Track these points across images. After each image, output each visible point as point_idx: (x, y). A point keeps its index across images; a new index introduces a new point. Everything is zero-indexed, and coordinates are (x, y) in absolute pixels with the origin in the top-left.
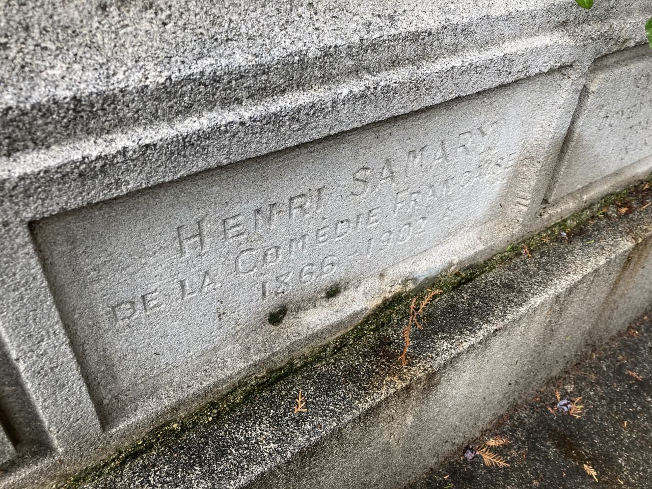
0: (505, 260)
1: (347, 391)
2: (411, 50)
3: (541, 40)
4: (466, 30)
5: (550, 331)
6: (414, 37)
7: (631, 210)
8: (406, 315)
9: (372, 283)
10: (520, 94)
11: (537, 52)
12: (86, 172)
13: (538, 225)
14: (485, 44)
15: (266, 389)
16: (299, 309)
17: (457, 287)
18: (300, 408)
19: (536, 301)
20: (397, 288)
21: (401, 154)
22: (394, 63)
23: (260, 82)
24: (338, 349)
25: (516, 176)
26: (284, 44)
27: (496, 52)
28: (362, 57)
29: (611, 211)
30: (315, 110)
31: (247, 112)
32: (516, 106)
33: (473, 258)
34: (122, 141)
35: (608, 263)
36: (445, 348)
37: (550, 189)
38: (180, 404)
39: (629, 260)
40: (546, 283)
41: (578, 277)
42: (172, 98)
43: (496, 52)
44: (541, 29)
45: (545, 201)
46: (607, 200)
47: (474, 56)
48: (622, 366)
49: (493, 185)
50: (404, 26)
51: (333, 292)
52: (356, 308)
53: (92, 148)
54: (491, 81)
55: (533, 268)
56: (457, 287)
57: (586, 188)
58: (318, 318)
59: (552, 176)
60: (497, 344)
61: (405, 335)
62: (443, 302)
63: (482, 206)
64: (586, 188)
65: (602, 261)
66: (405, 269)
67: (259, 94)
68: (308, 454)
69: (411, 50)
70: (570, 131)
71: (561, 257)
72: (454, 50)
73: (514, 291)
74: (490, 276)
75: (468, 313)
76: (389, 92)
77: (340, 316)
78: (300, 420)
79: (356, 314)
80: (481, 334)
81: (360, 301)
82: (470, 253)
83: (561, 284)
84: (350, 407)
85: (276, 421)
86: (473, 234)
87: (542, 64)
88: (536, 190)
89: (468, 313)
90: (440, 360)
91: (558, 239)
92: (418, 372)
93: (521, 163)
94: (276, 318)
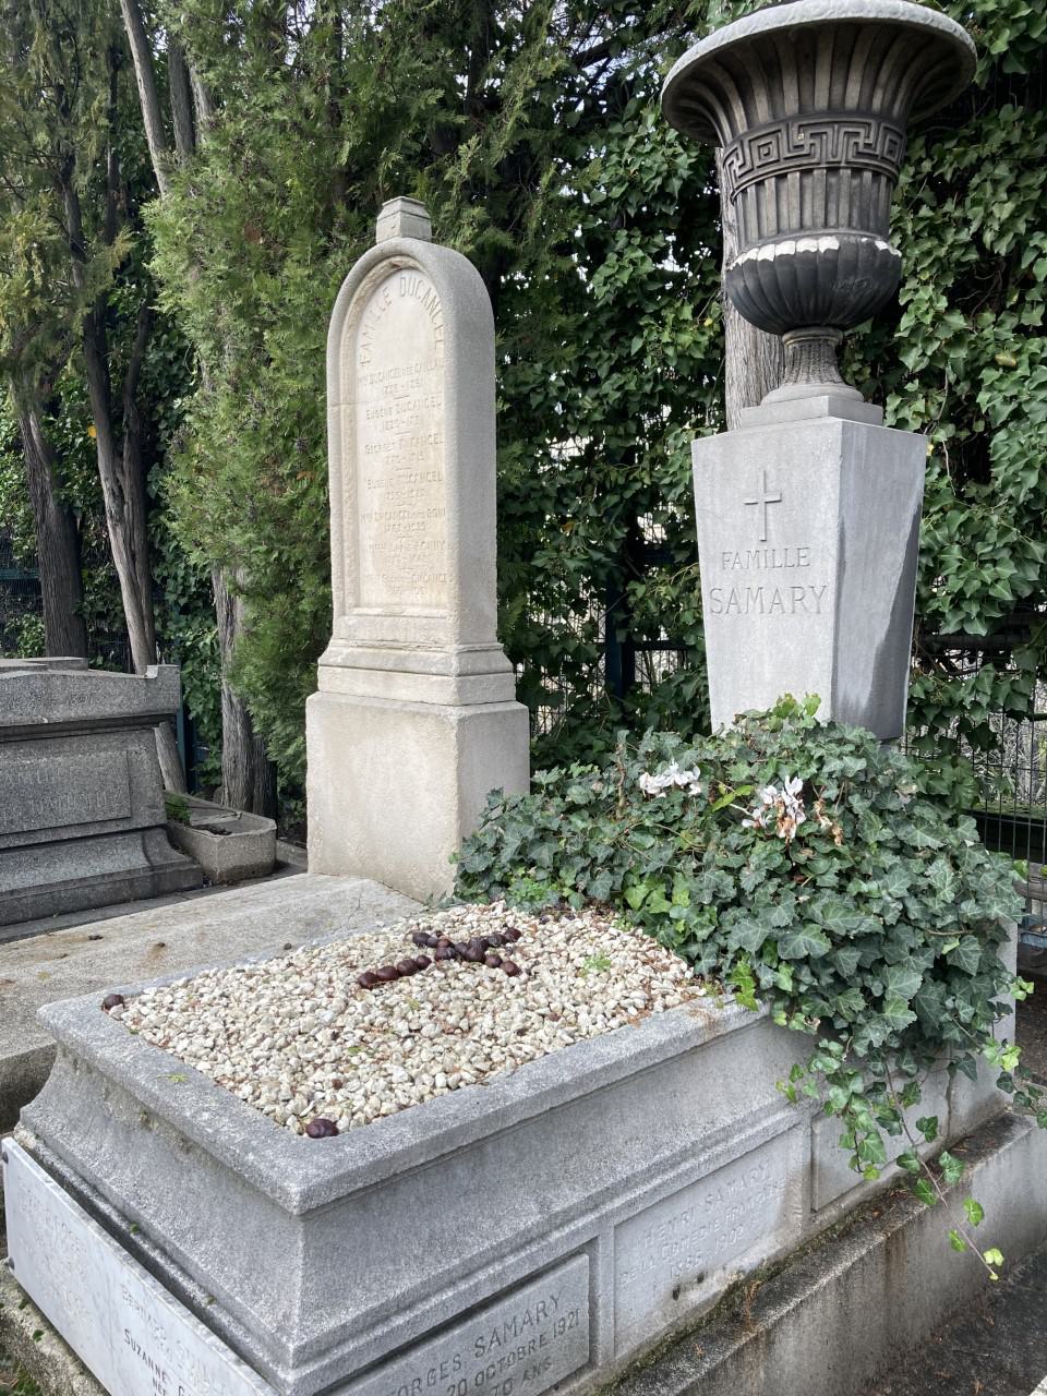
0: (798, 1258)
1: (722, 1341)
2: (723, 1135)
3: (779, 1116)
4: (743, 1121)
5: (845, 1316)
6: (724, 1129)
7: (882, 1213)
8: (743, 1299)
9: (719, 1274)
10: (776, 1143)
11: (779, 1122)
12: (631, 1204)
13: (814, 1229)
14: (752, 1125)
15: (679, 1342)
16: (686, 1290)
17: (771, 1278)
18: (699, 1352)
19: (824, 1281)
20: (735, 1277)
21: (724, 1185)
22: (717, 1143)
23: (673, 1163)
24: (709, 1322)
25: (788, 1194)
26: (679, 1144)
27: (759, 1128)
28: (706, 1144)
29: (868, 1215)
30: (693, 1169)
31: (672, 1174)
32: (776, 1151)
33: (776, 1255)
34: (639, 1192)
35: (869, 1252)
36: (773, 1315)
37: (812, 1202)
38: (641, 1346)
39: (888, 1252)
40: (828, 1270)
41: (849, 1264)
42: (649, 1174)
43: (759, 1128)
44: (778, 1110)
45: (813, 1210)
46: (862, 1206)
47: (750, 1132)
48: (931, 1368)
49: (775, 1199)
50: (719, 1126)
51: (701, 1279)
52: (715, 1290)
53: (630, 1196)
54: (760, 1141)
55: (818, 1262)
56: (771, 1278)
57: (842, 1196)
58: (695, 1296)
59: (810, 1189)
60: (805, 1312)
61: (747, 1310)
62: (764, 1289)
63: (772, 1217)
64: (842, 1196)
65: (864, 1252)
66: (736, 1264)
67: (673, 1166)
68: (712, 1375)
69: (723, 1135)
70: (813, 1159)
71: (836, 1252)
72: (741, 1130)
73: (809, 1277)
74: (791, 1270)
75: (781, 1293)
76: (718, 1156)
77: (707, 1296)
78: (702, 1357)
79: (715, 1295)
80: (792, 1305)
81: (716, 1286)
82: (773, 1251)
83: (838, 1270)
84: (727, 1348)
85: (688, 1359)
86: (772, 1238)
87: (783, 1127)
88: (804, 1202)
89: (781, 1293)
90: (771, 1321)
91: (831, 1240)
92: (760, 1328)
93: (788, 1185)
94: (675, 1294)
